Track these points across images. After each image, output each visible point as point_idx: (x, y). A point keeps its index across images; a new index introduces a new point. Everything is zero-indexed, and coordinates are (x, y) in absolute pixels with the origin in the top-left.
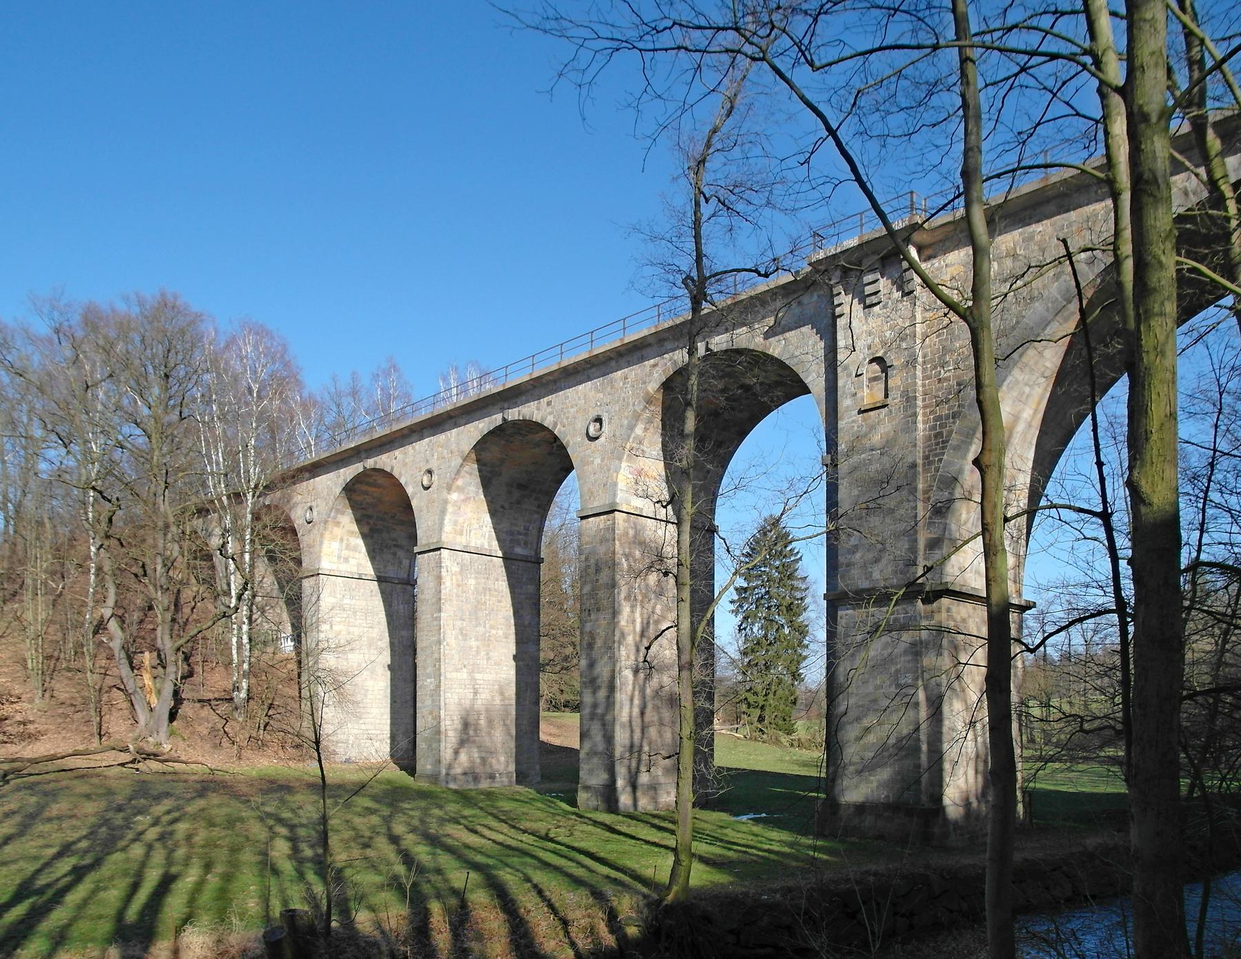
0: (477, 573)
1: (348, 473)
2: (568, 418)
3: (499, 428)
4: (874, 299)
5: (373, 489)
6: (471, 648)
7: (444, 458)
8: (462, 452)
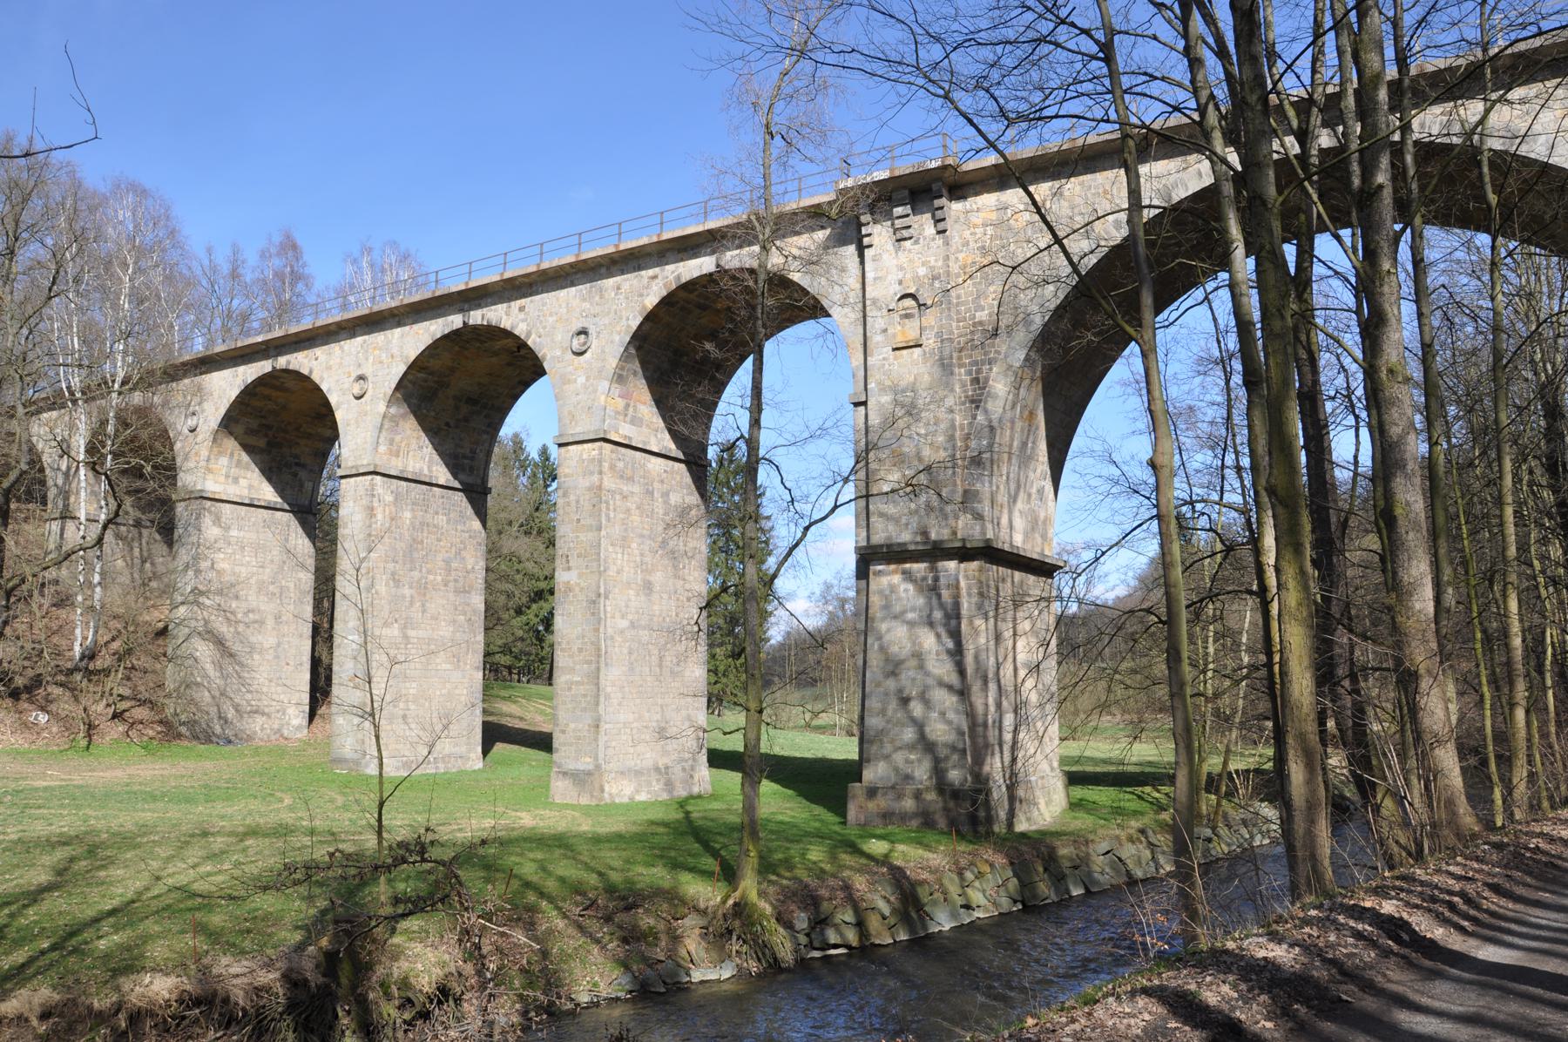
0: (413, 504)
1: (249, 373)
2: (544, 328)
3: (456, 333)
4: (905, 233)
5: (279, 393)
6: (404, 597)
7: (381, 362)
8: (407, 357)
